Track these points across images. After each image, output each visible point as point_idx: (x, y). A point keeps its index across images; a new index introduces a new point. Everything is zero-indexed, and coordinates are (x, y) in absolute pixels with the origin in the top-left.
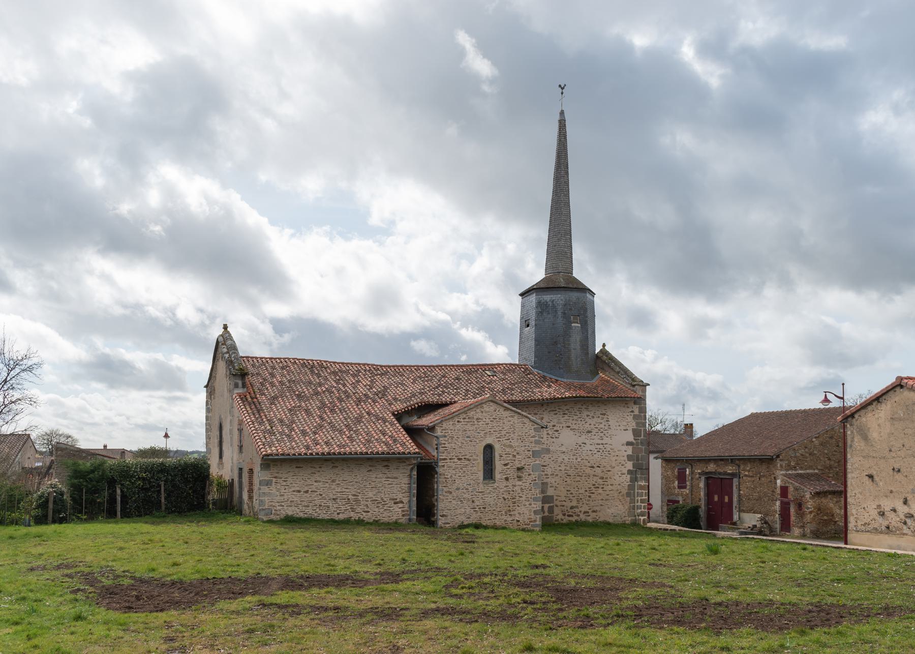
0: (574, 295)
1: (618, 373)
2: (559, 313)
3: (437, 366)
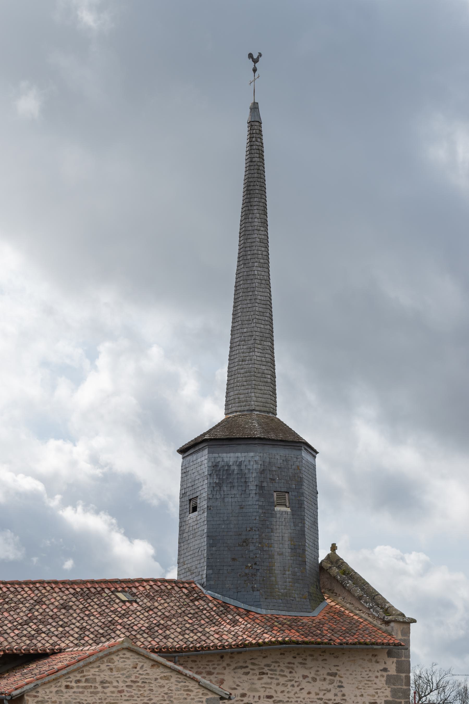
0: (279, 454)
1: (360, 598)
2: (252, 487)
3: (27, 583)
